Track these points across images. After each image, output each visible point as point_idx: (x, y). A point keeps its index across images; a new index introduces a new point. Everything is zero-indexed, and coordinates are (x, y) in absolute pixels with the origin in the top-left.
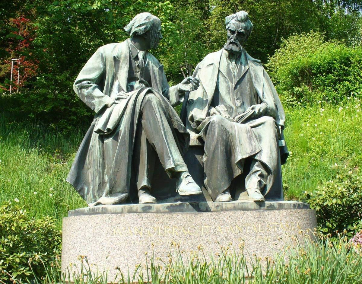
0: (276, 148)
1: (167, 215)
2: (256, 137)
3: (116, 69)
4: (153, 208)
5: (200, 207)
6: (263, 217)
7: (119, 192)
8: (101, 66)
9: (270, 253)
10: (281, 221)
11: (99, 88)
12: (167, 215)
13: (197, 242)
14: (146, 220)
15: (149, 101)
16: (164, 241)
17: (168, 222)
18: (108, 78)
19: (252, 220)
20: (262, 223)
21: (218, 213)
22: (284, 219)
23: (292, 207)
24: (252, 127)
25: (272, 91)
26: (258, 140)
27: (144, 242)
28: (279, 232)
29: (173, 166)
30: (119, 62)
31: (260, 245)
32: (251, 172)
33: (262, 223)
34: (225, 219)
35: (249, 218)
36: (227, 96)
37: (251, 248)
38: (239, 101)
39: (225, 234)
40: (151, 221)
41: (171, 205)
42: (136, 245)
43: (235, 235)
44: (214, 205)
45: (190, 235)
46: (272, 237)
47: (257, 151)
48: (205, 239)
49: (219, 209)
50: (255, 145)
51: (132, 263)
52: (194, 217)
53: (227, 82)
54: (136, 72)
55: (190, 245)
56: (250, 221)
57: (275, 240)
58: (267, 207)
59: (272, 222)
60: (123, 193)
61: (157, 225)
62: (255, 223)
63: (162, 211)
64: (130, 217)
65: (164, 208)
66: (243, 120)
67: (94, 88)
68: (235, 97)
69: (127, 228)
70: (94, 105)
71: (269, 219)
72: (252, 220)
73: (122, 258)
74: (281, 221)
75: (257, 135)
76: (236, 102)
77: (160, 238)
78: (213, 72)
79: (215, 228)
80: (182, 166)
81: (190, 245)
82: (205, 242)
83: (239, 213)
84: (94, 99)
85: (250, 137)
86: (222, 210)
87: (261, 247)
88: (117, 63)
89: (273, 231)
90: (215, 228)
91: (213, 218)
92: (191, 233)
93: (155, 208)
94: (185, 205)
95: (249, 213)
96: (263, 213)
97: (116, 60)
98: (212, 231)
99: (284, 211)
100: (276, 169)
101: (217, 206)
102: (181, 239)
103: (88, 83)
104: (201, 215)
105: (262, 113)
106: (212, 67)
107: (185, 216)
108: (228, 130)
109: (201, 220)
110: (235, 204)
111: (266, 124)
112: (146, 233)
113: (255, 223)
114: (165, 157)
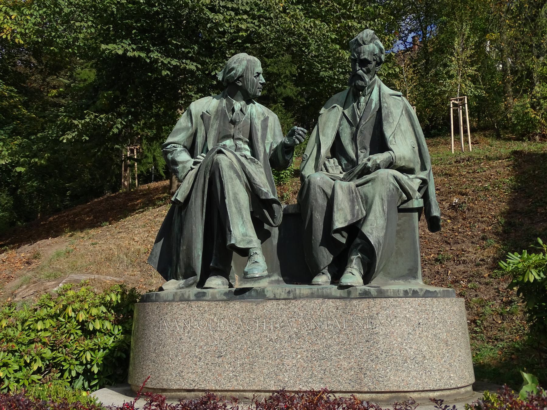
4: (207, 295)
5: (266, 293)
9: (359, 359)
12: (222, 303)
13: (257, 339)
14: (196, 309)
16: (216, 336)
20: (349, 316)
21: (288, 301)
23: (401, 295)
24: (357, 186)
26: (364, 202)
28: (374, 330)
32: (352, 247)
33: (349, 316)
34: (296, 310)
35: (330, 310)
37: (332, 351)
39: (295, 329)
40: (202, 311)
42: (182, 341)
43: (310, 331)
44: (284, 290)
45: (249, 330)
46: (363, 336)
48: (268, 336)
49: (291, 296)
51: (176, 364)
52: (255, 307)
56: (331, 314)
57: (367, 341)
58: (360, 293)
59: (363, 315)
61: (208, 316)
62: (338, 316)
63: (218, 298)
64: (178, 306)
65: (221, 295)
69: (174, 320)
71: (359, 312)
73: (166, 357)
75: (363, 196)
77: (212, 333)
81: (249, 342)
82: (268, 340)
83: (317, 302)
86: (295, 298)
87: (346, 350)
89: (365, 327)
91: (280, 308)
92: (251, 327)
93: (210, 295)
95: (330, 302)
98: (278, 325)
99: (371, 300)
101: (289, 292)
102: (237, 334)
104: (264, 304)
107: (244, 305)
109: (264, 311)
110: (313, 290)
113: (338, 316)
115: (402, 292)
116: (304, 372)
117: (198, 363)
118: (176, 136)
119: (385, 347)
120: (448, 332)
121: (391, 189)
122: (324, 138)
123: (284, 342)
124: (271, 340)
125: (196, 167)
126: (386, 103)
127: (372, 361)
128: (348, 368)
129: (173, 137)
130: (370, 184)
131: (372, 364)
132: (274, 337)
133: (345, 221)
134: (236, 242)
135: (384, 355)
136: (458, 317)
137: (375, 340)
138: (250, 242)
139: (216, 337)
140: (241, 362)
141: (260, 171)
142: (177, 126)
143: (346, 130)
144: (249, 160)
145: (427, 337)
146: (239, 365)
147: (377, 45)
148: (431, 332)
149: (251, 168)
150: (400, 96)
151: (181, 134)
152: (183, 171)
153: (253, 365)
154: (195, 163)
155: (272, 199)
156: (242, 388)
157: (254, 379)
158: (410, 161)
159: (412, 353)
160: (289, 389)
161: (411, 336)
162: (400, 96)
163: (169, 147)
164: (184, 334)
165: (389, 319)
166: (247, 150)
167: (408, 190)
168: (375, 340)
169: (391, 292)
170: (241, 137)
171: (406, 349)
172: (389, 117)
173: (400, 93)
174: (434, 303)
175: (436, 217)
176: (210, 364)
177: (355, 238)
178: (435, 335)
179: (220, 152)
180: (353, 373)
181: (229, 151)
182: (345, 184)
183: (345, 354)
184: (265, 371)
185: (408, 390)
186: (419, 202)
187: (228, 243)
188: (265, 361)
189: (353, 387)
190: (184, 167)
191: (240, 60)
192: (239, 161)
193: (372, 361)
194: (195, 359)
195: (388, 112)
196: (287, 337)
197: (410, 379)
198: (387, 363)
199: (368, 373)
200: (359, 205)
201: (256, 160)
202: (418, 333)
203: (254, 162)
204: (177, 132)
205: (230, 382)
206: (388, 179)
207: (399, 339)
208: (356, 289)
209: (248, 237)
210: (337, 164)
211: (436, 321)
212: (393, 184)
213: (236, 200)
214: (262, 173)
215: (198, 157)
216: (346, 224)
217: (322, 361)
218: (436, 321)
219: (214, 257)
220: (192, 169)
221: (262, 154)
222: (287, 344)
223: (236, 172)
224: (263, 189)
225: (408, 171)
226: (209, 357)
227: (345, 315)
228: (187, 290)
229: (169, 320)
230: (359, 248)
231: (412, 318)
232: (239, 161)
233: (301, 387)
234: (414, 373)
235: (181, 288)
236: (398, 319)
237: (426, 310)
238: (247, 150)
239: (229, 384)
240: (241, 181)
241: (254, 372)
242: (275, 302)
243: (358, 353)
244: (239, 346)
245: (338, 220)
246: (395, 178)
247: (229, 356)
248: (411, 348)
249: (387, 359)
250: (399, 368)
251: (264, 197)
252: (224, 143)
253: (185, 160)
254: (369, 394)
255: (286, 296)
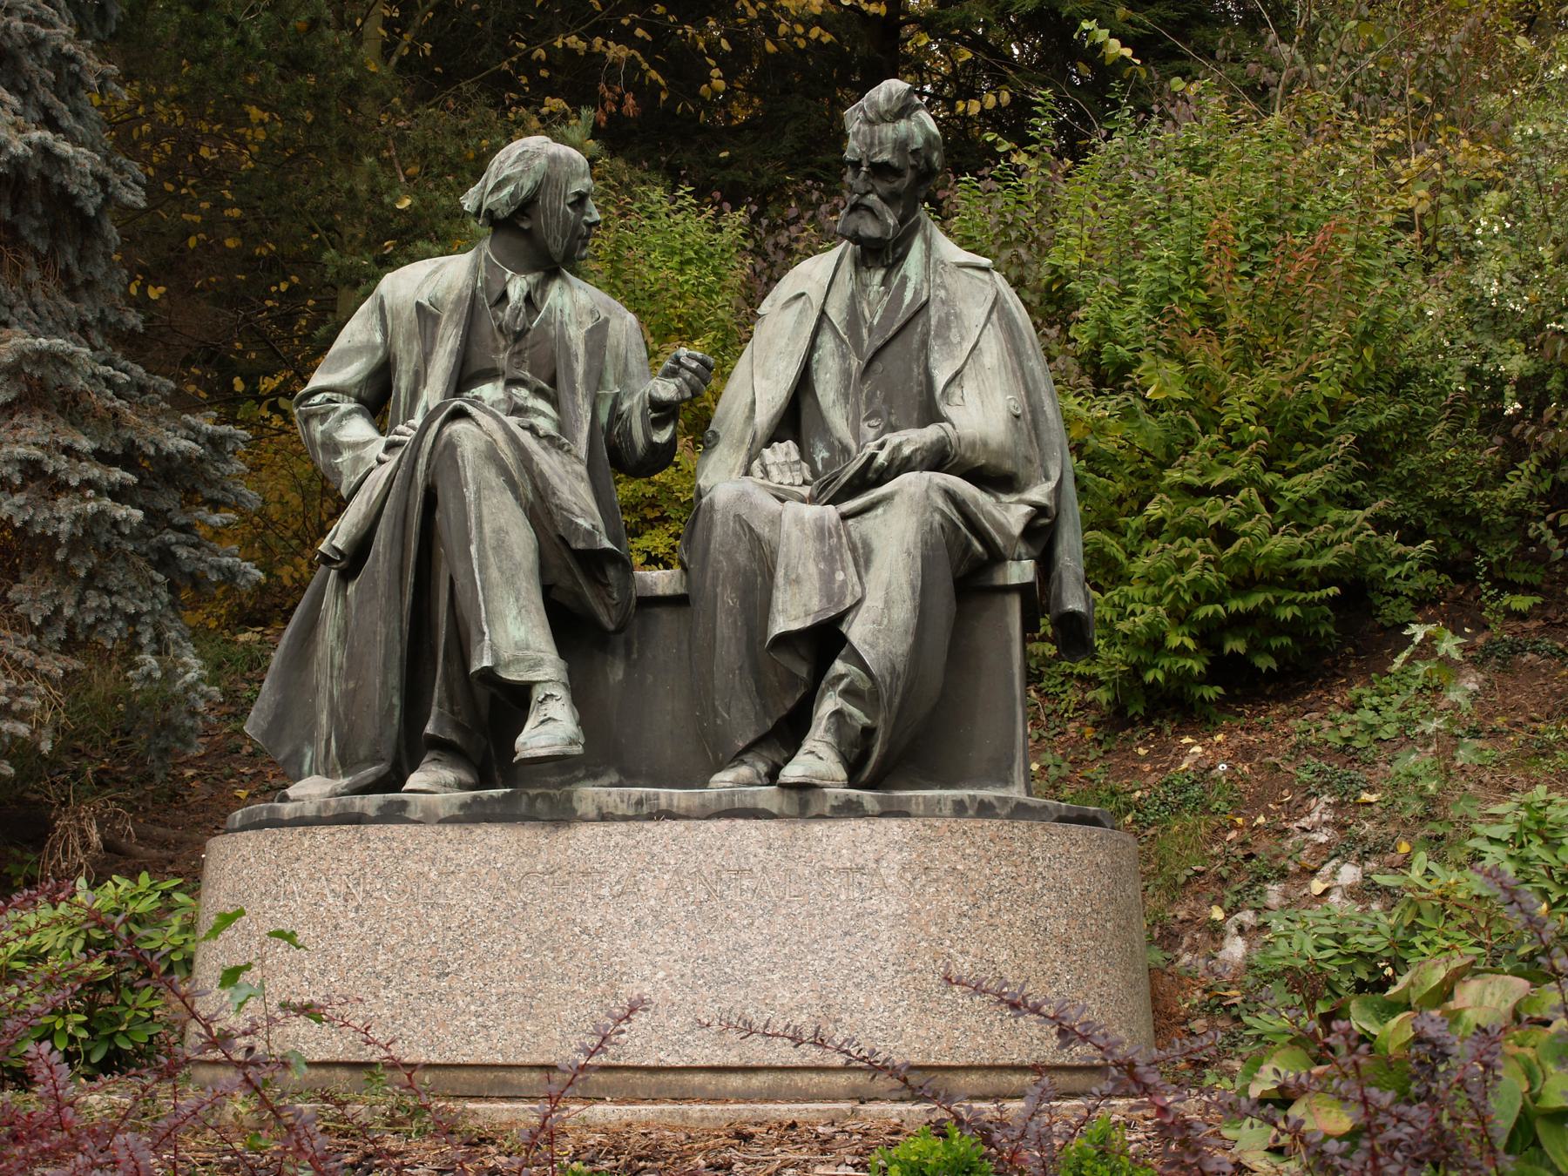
0: (913, 588)
1: (451, 831)
2: (853, 549)
3: (424, 343)
5: (575, 804)
6: (806, 845)
7: (366, 760)
8: (378, 338)
9: (823, 982)
10: (877, 861)
11: (364, 415)
14: (381, 846)
15: (451, 446)
16: (435, 921)
17: (452, 854)
18: (403, 382)
19: (761, 855)
20: (800, 867)
22: (892, 854)
24: (844, 517)
25: (1023, 375)
27: (367, 924)
28: (866, 904)
29: (487, 662)
30: (436, 319)
31: (786, 951)
32: (823, 685)
33: (800, 867)
35: (751, 849)
36: (838, 407)
38: (873, 422)
39: (652, 902)
41: (475, 798)
43: (691, 908)
47: (848, 602)
50: (844, 582)
52: (543, 841)
53: (844, 357)
54: (496, 350)
55: (523, 937)
56: (752, 860)
57: (846, 934)
60: (374, 760)
61: (413, 866)
62: (771, 866)
66: (833, 489)
67: (350, 413)
68: (863, 407)
70: (340, 473)
71: (828, 856)
72: (761, 855)
73: (295, 977)
74: (877, 861)
75: (859, 545)
76: (864, 426)
78: (799, 323)
79: (618, 882)
80: (537, 664)
81: (523, 937)
82: (577, 930)
84: (340, 454)
85: (831, 554)
88: (429, 323)
90: (618, 882)
91: (612, 843)
94: (525, 798)
96: (807, 829)
97: (426, 316)
98: (605, 891)
99: (862, 823)
100: (900, 667)
101: (640, 803)
102: (493, 916)
103: (330, 401)
105: (908, 459)
106: (799, 305)
108: (758, 530)
111: (897, 499)
112: (376, 894)
114: (474, 631)
115: (949, 804)
116: (672, 1016)
117: (382, 993)
118: (337, 370)
119: (895, 950)
120: (1071, 916)
121: (936, 525)
122: (765, 383)
123: (621, 934)
124: (585, 931)
125: (392, 460)
126: (944, 287)
127: (857, 985)
128: (792, 1005)
129: (329, 372)
130: (880, 511)
131: (856, 993)
132: (593, 922)
133: (807, 614)
134: (497, 664)
135: (891, 970)
136: (1106, 881)
137: (868, 931)
138: (537, 664)
139: (433, 922)
140: (502, 990)
141: (574, 471)
142: (342, 341)
143: (830, 363)
144: (545, 442)
145: (1011, 925)
146: (494, 999)
147: (922, 124)
148: (1022, 911)
149: (548, 462)
150: (986, 269)
151: (351, 363)
152: (354, 471)
153: (532, 997)
154: (390, 447)
155: (606, 551)
156: (500, 1061)
157: (536, 1035)
158: (1002, 452)
159: (966, 966)
160: (631, 1062)
161: (965, 921)
162: (986, 269)
163: (317, 399)
164: (345, 914)
165: (909, 876)
166: (544, 415)
167: (988, 533)
168: (868, 931)
169: (917, 804)
170: (527, 375)
171: (949, 956)
172: (949, 328)
173: (986, 262)
174: (1035, 836)
175: (1074, 615)
176: (415, 994)
177: (832, 662)
178: (1034, 923)
179: (459, 414)
180: (804, 1017)
181: (485, 410)
182: (811, 511)
183: (786, 967)
184: (567, 1014)
185: (954, 1063)
186: (1023, 570)
187: (476, 666)
188: (566, 987)
189: (804, 1055)
190: (358, 460)
191: (527, 155)
192: (513, 439)
193: (857, 985)
194: (374, 982)
195: (948, 314)
196: (629, 921)
197: (957, 1033)
198: (899, 991)
199: (845, 1017)
200: (843, 569)
201: (564, 440)
202: (985, 911)
203: (561, 447)
204: (341, 358)
205: (469, 1042)
206: (928, 497)
207: (933, 929)
208: (825, 794)
209: (529, 653)
210: (795, 456)
211: (1038, 886)
212: (943, 514)
213: (500, 547)
214: (578, 476)
215: (400, 428)
216: (809, 622)
217: (723, 987)
218: (1038, 886)
219: (435, 710)
220: (381, 462)
221: (586, 428)
222: (627, 944)
223: (503, 470)
224: (580, 521)
225: (997, 480)
226: (412, 977)
227: (792, 865)
228: (357, 799)
229: (303, 875)
230: (841, 686)
231: (971, 874)
232: (513, 439)
233: (662, 1055)
234: (970, 1021)
235: (337, 795)
236: (933, 875)
237: (1012, 853)
238: (544, 415)
239: (466, 1050)
240: (517, 498)
241: (536, 1017)
242: (599, 828)
243: (820, 965)
244: (497, 948)
245: (785, 611)
246: (950, 495)
247: (467, 974)
248: (963, 952)
249: (897, 981)
250: (930, 1006)
251: (581, 545)
252: (476, 391)
253: (361, 439)
254: (845, 1076)
255: (631, 812)
